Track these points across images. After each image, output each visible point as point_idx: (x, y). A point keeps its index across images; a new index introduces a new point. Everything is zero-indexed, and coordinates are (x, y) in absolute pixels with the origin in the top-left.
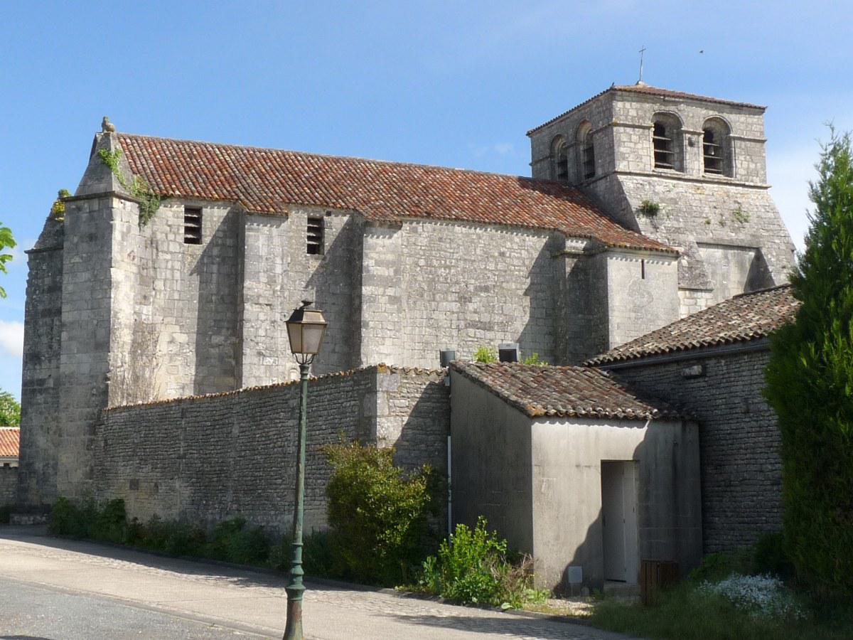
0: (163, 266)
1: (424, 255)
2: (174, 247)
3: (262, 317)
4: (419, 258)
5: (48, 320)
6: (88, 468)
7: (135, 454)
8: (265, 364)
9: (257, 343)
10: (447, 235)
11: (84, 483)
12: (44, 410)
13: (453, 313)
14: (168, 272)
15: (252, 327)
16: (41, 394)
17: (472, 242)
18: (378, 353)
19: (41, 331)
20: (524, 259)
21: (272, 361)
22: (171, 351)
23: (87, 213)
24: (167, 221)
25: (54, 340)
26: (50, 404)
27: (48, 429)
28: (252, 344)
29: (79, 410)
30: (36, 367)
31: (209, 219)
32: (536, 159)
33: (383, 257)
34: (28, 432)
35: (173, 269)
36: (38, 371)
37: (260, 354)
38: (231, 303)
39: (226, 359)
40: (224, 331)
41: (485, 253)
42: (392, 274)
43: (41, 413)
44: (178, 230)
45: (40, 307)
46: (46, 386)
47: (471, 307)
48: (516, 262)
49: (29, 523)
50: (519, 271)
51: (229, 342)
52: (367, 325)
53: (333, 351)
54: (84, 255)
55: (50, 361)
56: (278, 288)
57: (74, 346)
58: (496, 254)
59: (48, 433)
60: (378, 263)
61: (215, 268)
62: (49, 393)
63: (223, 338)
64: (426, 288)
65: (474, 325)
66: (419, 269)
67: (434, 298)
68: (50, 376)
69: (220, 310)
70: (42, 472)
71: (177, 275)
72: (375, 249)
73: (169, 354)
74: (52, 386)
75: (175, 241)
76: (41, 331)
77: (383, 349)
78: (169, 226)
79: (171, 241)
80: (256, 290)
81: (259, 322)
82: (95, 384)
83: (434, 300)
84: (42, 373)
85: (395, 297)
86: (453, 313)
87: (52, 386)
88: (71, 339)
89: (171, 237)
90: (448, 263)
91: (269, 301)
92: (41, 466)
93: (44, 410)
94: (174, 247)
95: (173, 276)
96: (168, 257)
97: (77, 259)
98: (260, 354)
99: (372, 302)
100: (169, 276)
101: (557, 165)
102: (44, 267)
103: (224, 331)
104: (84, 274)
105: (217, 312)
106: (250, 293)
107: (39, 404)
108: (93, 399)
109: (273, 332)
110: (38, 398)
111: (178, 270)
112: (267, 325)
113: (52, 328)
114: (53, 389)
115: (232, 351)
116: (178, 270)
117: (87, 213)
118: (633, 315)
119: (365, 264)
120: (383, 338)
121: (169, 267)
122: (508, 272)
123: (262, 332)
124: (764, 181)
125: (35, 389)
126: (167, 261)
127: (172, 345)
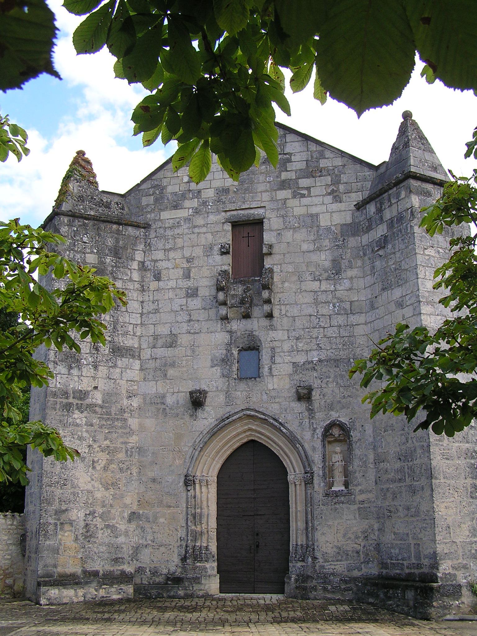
11: (471, 543)
12: (85, 434)
26: (96, 427)
27: (93, 461)
29: (457, 444)
30: (72, 371)
36: (76, 378)
46: (88, 401)
55: (96, 367)
59: (94, 468)
62: (95, 412)
68: (96, 388)
70: (82, 524)
74: (100, 402)
87: (100, 402)
92: (81, 515)
93: (85, 434)
102: (85, 239)
107: (77, 425)
110: (75, 416)
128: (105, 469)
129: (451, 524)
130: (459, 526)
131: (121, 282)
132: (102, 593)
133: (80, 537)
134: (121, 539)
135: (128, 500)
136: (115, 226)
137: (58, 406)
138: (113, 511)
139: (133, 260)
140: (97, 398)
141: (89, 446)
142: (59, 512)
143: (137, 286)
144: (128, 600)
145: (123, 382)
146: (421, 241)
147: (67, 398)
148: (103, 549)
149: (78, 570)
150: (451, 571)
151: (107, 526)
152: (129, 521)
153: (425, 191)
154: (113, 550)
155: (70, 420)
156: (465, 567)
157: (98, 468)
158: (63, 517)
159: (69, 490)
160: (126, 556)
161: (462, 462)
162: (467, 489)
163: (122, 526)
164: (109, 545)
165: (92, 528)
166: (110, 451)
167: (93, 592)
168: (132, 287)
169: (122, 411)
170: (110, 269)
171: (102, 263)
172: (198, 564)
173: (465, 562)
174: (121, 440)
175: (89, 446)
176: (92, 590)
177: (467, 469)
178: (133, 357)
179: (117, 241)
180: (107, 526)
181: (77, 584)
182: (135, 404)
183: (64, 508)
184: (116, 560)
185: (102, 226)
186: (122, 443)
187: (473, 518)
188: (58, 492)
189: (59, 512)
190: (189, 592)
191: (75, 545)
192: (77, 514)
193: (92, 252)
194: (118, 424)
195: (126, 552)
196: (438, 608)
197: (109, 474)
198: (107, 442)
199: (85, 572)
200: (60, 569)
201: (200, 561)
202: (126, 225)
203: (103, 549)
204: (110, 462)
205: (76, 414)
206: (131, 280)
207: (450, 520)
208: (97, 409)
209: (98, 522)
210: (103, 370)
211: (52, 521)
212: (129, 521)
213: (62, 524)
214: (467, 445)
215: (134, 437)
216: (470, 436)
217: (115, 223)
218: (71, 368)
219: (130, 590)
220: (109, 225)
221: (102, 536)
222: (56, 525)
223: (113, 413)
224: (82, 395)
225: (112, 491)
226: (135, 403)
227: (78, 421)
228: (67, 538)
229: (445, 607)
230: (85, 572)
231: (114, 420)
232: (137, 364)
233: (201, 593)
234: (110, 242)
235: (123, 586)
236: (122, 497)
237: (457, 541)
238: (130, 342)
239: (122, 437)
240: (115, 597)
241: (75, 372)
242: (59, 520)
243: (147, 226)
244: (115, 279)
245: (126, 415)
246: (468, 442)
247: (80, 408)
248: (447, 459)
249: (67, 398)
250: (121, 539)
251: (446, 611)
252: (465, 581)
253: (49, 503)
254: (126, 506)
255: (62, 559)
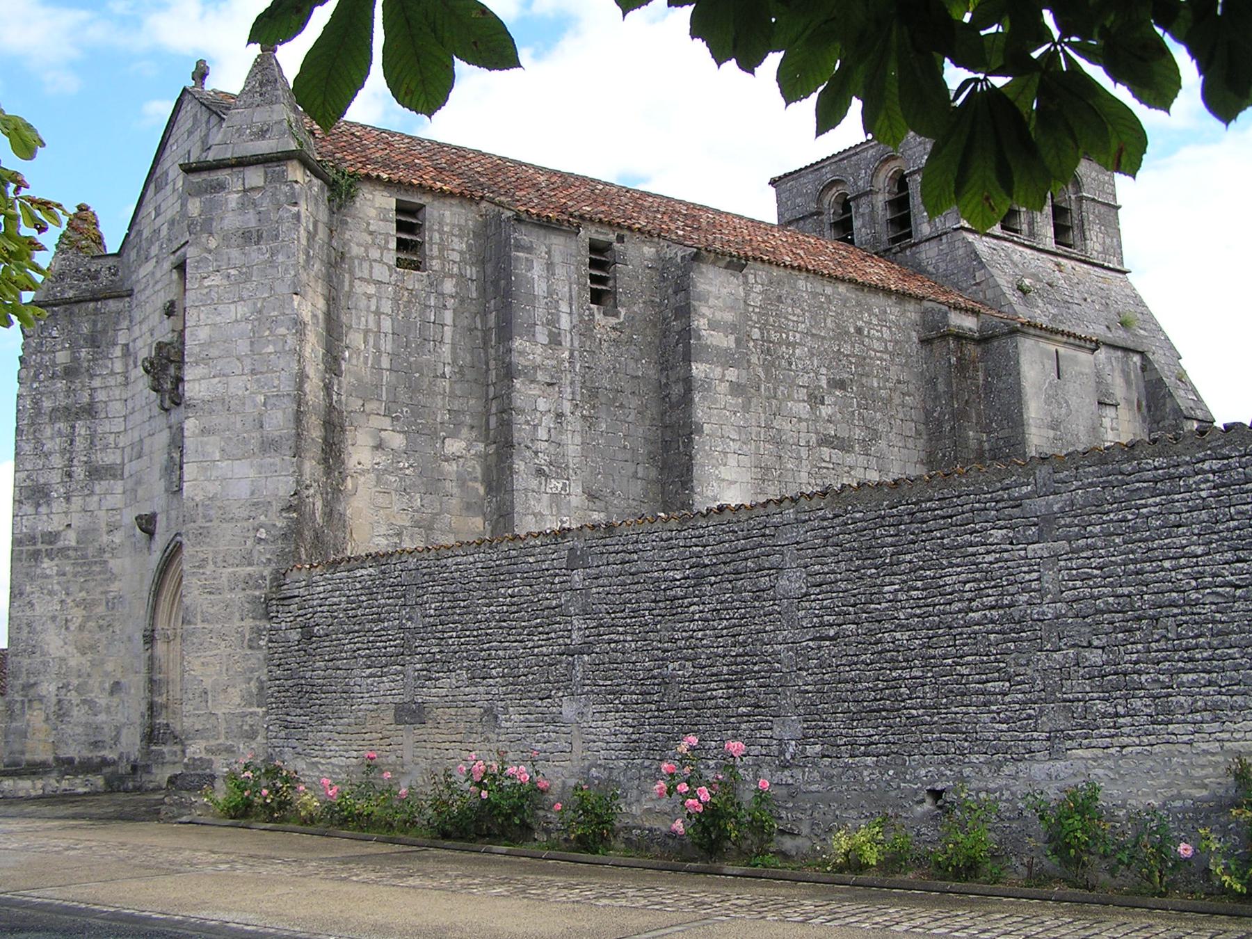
0: (363, 303)
1: (759, 322)
2: (381, 273)
3: (542, 405)
4: (752, 327)
5: (62, 425)
6: (253, 686)
7: (407, 650)
8: (548, 490)
9: (536, 453)
10: (788, 293)
11: (244, 715)
12: (56, 587)
13: (800, 420)
14: (371, 317)
15: (528, 423)
16: (52, 560)
17: (821, 307)
18: (718, 478)
19: (49, 446)
20: (885, 341)
21: (560, 486)
22: (378, 464)
23: (238, 192)
24: (368, 224)
25: (75, 462)
26: (69, 576)
27: (67, 620)
28: (528, 453)
29: (230, 570)
30: (40, 509)
31: (436, 227)
32: (787, 216)
33: (718, 315)
34: (24, 627)
35: (378, 313)
36: (45, 518)
37: (540, 472)
38: (476, 381)
39: (470, 484)
40: (465, 431)
41: (838, 326)
42: (733, 345)
43: (51, 593)
44: (387, 242)
45: (47, 404)
46: (60, 544)
47: (825, 411)
48: (876, 345)
49: (33, 793)
50: (881, 359)
51: (473, 452)
52: (700, 430)
53: (635, 476)
54: (233, 272)
55: (68, 500)
56: (566, 355)
57: (213, 446)
58: (852, 330)
59: (67, 628)
60: (713, 325)
61: (448, 316)
62: (68, 557)
63: (463, 444)
64: (763, 376)
65: (825, 441)
66: (752, 344)
67: (775, 393)
68: (69, 526)
69: (458, 393)
70: (54, 700)
71: (387, 325)
72: (707, 301)
73: (374, 469)
74: (73, 544)
75: (381, 261)
76: (49, 446)
77: (725, 473)
78: (371, 233)
79: (375, 261)
80: (531, 357)
81: (538, 414)
82: (262, 518)
83: (775, 397)
84: (52, 520)
85: (739, 385)
86: (800, 420)
87: (73, 544)
88: (204, 431)
89: (375, 254)
90: (791, 338)
91: (552, 377)
92: (53, 688)
93: (56, 587)
94: (381, 273)
95: (379, 326)
96: (371, 289)
97: (216, 280)
98: (540, 472)
99: (705, 390)
100: (372, 325)
101: (827, 226)
102: (55, 333)
103: (465, 431)
104: (232, 307)
105: (453, 396)
106: (522, 361)
107: (47, 577)
108: (261, 548)
109: (561, 433)
110: (45, 565)
111: (387, 315)
112: (548, 421)
113: (72, 441)
114: (76, 549)
115: (478, 469)
116: (387, 315)
117: (238, 192)
118: (1051, 433)
119: (694, 324)
120: (726, 453)
121: (373, 308)
122: (868, 360)
123: (542, 433)
124: (1121, 263)
125: (39, 551)
126: (369, 297)
127: (379, 453)
128: (81, 628)
129: (209, 688)
130: (225, 691)
131: (99, 379)
132: (65, 784)
133: (51, 716)
134: (102, 717)
135: (109, 667)
136: (91, 305)
137: (24, 556)
138: (91, 682)
139: (115, 344)
140: (71, 539)
141: (62, 601)
142: (28, 687)
143: (120, 379)
144: (96, 793)
145: (102, 514)
146: (197, 268)
147: (35, 544)
148: (79, 730)
149: (49, 757)
150: (203, 755)
151: (84, 702)
152: (112, 693)
153: (214, 184)
154: (91, 731)
155: (39, 571)
156: (229, 750)
157: (72, 628)
158: (32, 692)
159: (38, 658)
160: (107, 739)
161: (238, 596)
162: (244, 636)
163: (102, 701)
164: (87, 725)
165: (66, 705)
166: (85, 604)
167: (52, 783)
168: (113, 383)
169: (102, 550)
170: (85, 364)
171: (75, 359)
172: (154, 748)
173: (230, 742)
174: (101, 589)
175: (62, 601)
176: (53, 782)
177: (247, 605)
178: (114, 477)
179: (95, 323)
180: (84, 702)
181: (34, 773)
182: (117, 540)
183: (32, 681)
184: (96, 744)
185: (76, 309)
186: (102, 593)
187: (251, 679)
188: (26, 662)
189: (28, 687)
190: (138, 784)
191: (45, 726)
192: (48, 688)
193: (64, 348)
194: (96, 568)
195: (107, 734)
196: (171, 805)
197: (86, 634)
198: (83, 594)
199: (57, 759)
200: (28, 757)
201: (155, 744)
202: (106, 298)
203: (79, 730)
204: (87, 618)
205: (46, 563)
206: (112, 373)
207: (208, 683)
208: (71, 553)
209: (73, 696)
210: (77, 501)
211: (20, 699)
212: (112, 693)
213: (30, 701)
214: (249, 568)
215: (117, 583)
216: (255, 554)
217: (91, 300)
218: (39, 505)
219: (99, 781)
220: (84, 305)
221: (78, 714)
222: (23, 702)
223: (90, 555)
224: (52, 537)
225: (89, 656)
226: (118, 538)
227: (48, 572)
228: (36, 718)
229: (182, 805)
230: (57, 759)
231: (90, 564)
232: (119, 486)
233: (151, 786)
234: (85, 329)
235: (90, 777)
236: (102, 662)
237: (220, 713)
238: (111, 458)
239: (101, 585)
240: (81, 790)
241: (43, 509)
242: (26, 696)
243: (130, 294)
244: (92, 377)
245: (107, 556)
246: (250, 564)
247: (49, 555)
248: (210, 593)
249: (35, 544)
250: (102, 717)
251: (183, 810)
252: (226, 770)
253: (16, 677)
254: (107, 674)
255: (30, 743)
